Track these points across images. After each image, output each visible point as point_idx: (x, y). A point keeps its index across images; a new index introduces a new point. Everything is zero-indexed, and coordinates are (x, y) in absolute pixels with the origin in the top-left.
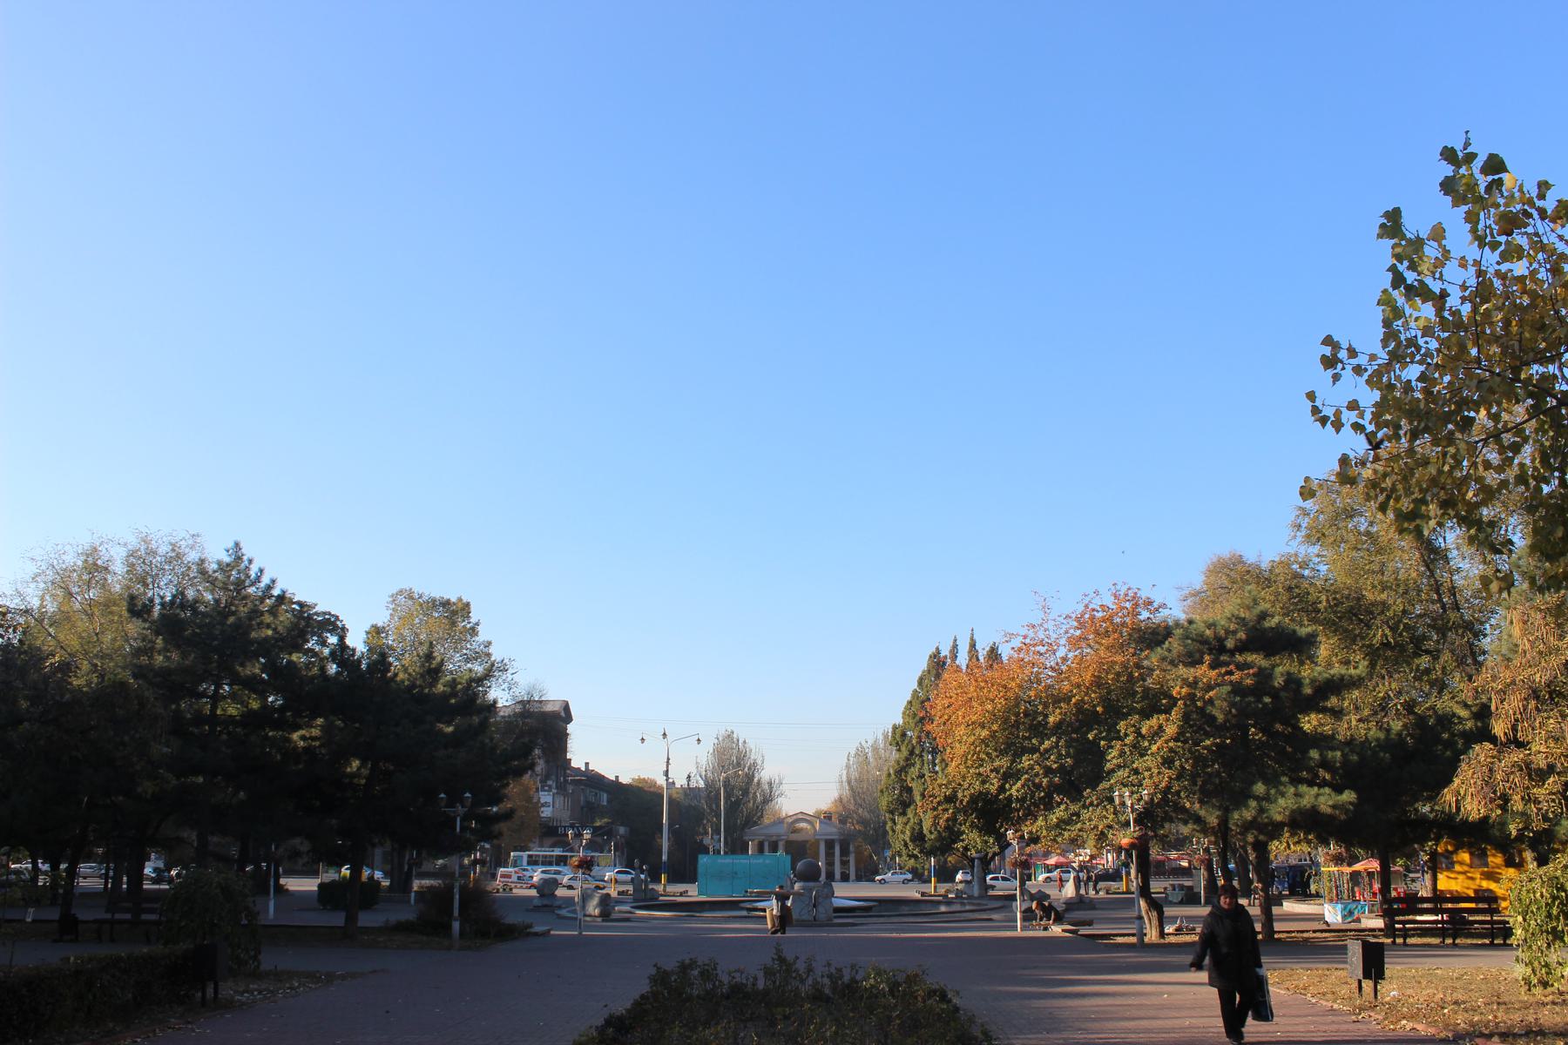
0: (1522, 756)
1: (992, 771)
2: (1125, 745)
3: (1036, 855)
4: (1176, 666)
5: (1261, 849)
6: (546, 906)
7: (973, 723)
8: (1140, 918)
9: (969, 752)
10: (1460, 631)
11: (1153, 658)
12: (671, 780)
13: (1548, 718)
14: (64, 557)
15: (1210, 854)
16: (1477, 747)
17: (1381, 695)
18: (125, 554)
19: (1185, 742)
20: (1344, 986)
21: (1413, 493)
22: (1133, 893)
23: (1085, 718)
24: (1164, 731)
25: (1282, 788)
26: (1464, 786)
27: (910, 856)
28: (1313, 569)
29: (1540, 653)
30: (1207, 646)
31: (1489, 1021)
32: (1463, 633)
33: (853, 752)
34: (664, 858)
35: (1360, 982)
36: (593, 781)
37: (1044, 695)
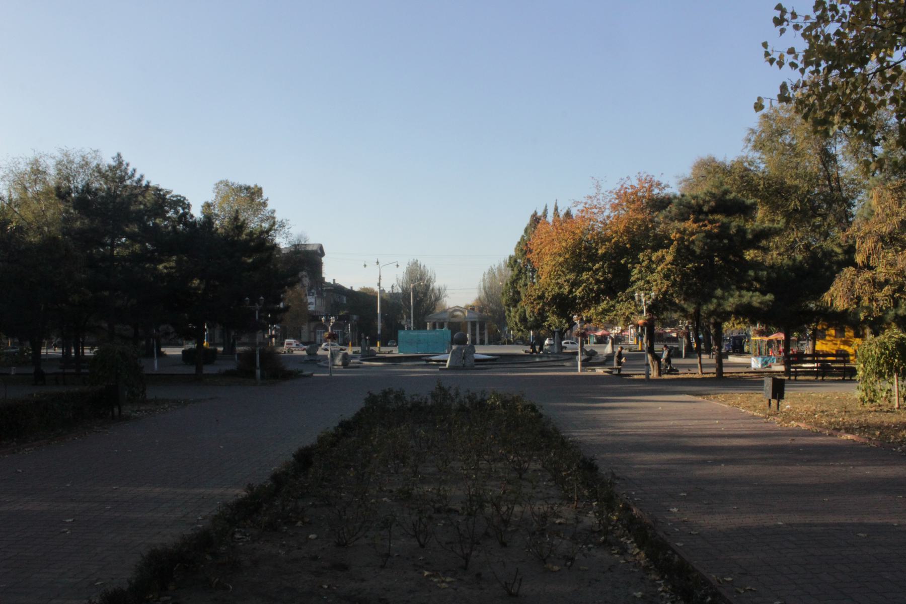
0: (871, 274)
1: (565, 281)
2: (642, 267)
3: (590, 329)
4: (674, 221)
5: (718, 326)
6: (312, 360)
7: (554, 254)
8: (648, 365)
9: (552, 271)
10: (840, 203)
11: (660, 217)
12: (382, 289)
13: (888, 253)
14: (19, 166)
15: (689, 329)
16: (845, 270)
17: (792, 240)
18: (55, 163)
19: (677, 265)
20: (761, 403)
21: (825, 108)
22: (644, 351)
23: (619, 251)
24: (665, 259)
25: (731, 292)
26: (836, 292)
27: (519, 330)
28: (756, 167)
29: (887, 215)
30: (692, 210)
31: (840, 421)
32: (842, 204)
33: (487, 272)
34: (379, 332)
35: (770, 400)
36: (338, 290)
37: (596, 237)
